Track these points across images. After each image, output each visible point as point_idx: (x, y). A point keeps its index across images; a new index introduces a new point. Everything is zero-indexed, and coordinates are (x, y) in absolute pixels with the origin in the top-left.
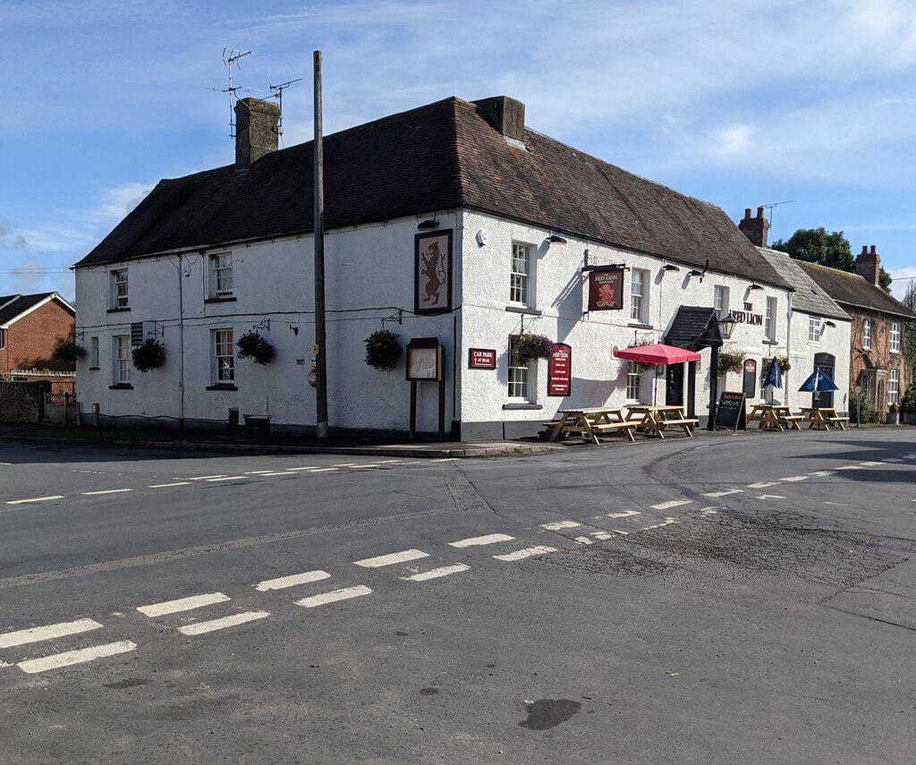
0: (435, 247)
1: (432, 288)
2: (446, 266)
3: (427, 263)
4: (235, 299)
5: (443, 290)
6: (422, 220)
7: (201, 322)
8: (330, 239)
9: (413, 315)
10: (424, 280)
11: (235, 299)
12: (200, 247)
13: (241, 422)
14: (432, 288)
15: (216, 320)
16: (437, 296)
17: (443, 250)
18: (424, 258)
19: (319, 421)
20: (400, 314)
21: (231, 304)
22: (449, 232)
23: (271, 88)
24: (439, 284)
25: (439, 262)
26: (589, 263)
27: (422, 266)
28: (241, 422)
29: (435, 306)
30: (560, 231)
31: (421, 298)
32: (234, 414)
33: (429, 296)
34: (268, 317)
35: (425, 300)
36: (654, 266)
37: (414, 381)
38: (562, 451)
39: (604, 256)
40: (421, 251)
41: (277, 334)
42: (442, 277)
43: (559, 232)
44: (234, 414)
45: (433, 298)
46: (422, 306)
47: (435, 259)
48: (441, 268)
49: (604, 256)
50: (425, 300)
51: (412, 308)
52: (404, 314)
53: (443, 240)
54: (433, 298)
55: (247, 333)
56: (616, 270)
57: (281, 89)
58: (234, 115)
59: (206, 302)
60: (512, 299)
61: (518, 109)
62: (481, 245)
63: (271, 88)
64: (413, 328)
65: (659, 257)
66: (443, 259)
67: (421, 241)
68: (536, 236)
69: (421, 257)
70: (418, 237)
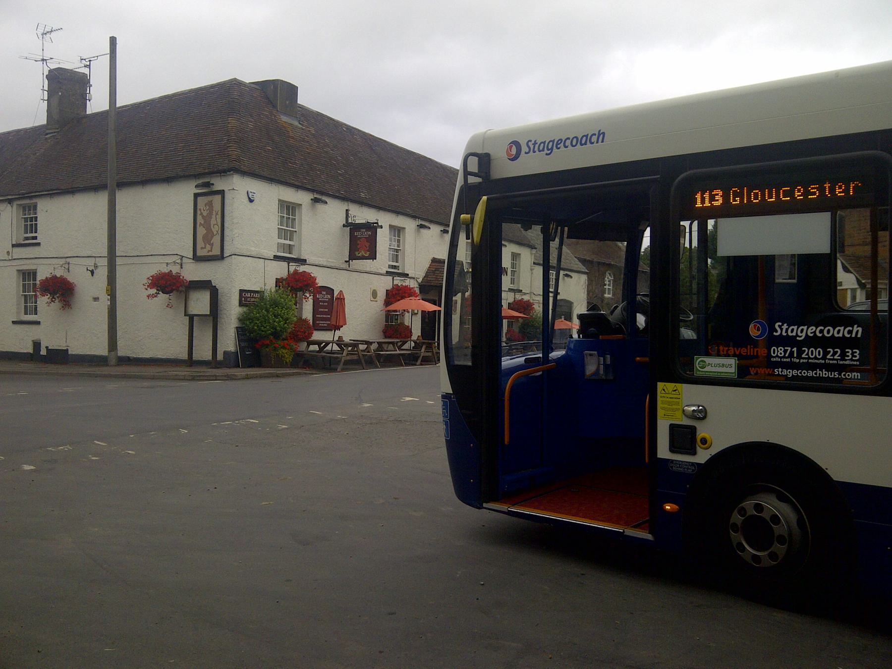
0: (210, 204)
1: (208, 239)
2: (219, 220)
3: (203, 216)
4: (39, 244)
5: (217, 240)
6: (200, 181)
7: (9, 263)
8: (126, 199)
9: (192, 261)
10: (201, 231)
11: (39, 244)
12: (10, 197)
13: (43, 352)
14: (208, 239)
15: (22, 262)
16: (212, 245)
17: (217, 206)
18: (201, 214)
19: (110, 351)
20: (182, 259)
21: (36, 248)
22: (222, 193)
23: (82, 59)
24: (213, 235)
25: (214, 216)
26: (350, 221)
27: (200, 219)
28: (43, 352)
29: (210, 254)
30: (322, 193)
31: (199, 247)
32: (37, 345)
33: (205, 246)
34: (68, 260)
35: (202, 248)
36: (409, 225)
37: (191, 318)
38: (312, 374)
39: (363, 215)
40: (198, 207)
41: (78, 276)
42: (216, 229)
43: (320, 194)
44: (37, 345)
45: (208, 247)
46: (200, 253)
47: (210, 214)
48: (215, 221)
49: (363, 215)
50: (202, 248)
51: (191, 255)
52: (184, 260)
53: (218, 198)
54: (208, 247)
55: (49, 276)
56: (372, 228)
57: (90, 61)
58: (46, 82)
59: (13, 246)
60: (511, 284)
61: (291, 90)
62: (251, 201)
63: (82, 59)
64: (193, 272)
65: (414, 217)
66: (217, 214)
67: (199, 199)
68: (303, 198)
69: (199, 212)
70: (196, 196)
